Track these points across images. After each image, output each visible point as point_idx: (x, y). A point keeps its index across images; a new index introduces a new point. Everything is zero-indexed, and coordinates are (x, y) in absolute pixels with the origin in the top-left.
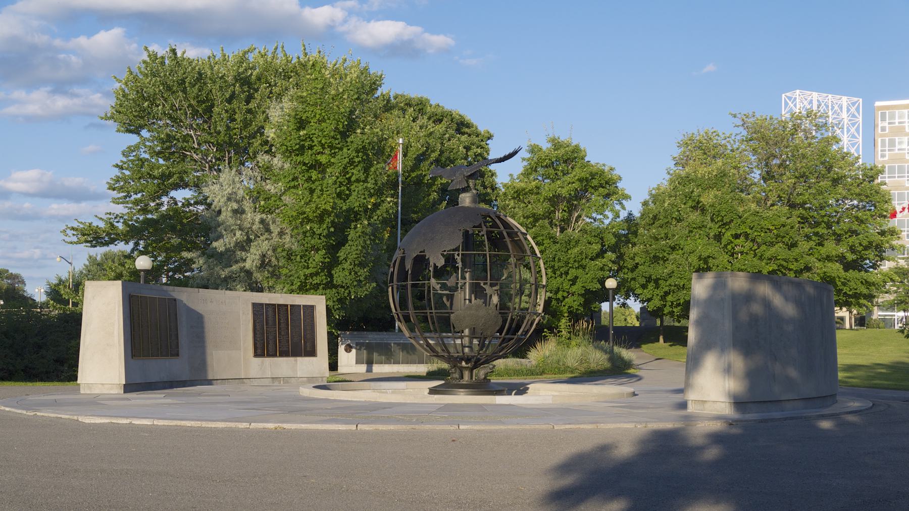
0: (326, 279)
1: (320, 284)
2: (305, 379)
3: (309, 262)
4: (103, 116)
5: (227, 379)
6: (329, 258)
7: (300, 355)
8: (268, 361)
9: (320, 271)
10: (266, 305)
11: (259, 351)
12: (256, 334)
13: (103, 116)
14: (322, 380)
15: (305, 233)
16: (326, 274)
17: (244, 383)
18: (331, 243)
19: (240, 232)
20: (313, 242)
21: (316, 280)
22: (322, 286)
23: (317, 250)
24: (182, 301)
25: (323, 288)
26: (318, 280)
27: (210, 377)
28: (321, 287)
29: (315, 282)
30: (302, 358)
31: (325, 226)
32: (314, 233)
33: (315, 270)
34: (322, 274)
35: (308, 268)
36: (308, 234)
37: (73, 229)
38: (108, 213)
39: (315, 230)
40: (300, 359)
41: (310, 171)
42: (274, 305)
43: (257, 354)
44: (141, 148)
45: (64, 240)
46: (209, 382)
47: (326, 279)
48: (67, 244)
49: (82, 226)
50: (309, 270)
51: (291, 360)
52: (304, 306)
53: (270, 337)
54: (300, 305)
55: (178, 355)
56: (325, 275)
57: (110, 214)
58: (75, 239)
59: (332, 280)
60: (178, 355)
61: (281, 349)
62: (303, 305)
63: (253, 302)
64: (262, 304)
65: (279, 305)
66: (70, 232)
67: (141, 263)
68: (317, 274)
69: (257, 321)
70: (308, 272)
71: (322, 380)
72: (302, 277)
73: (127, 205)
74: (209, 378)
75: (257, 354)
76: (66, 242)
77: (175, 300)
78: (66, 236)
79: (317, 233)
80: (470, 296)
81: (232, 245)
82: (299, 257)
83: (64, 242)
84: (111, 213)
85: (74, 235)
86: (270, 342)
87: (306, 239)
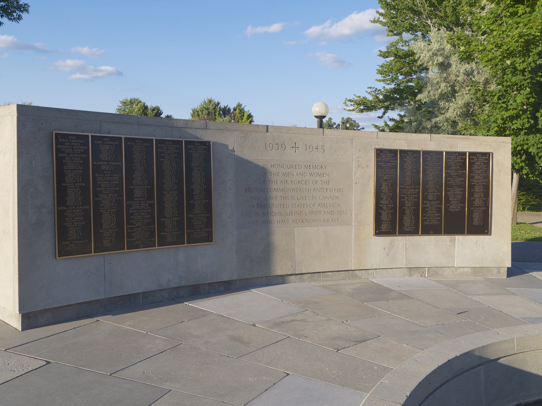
0: (529, 122)
1: (522, 129)
2: (469, 269)
3: (509, 104)
4: (372, 20)
5: (323, 272)
6: (533, 97)
7: (461, 232)
8: (401, 241)
9: (521, 113)
10: (402, 152)
11: (384, 227)
12: (382, 199)
13: (372, 20)
14: (499, 272)
15: (504, 70)
16: (529, 116)
17: (356, 276)
18: (537, 80)
19: (445, 84)
20: (514, 79)
21: (517, 124)
22: (524, 131)
23: (519, 90)
24: (226, 146)
25: (525, 134)
26: (518, 124)
27: (279, 269)
28: (522, 133)
29: (514, 127)
30: (442, 237)
31: (531, 59)
32: (515, 69)
33: (515, 112)
34: (524, 116)
35: (507, 110)
36: (508, 71)
37: (350, 101)
38: (369, 88)
39: (517, 65)
40: (459, 238)
41: (516, 6)
42: (417, 152)
43: (379, 232)
44: (400, 43)
45: (344, 109)
46: (282, 280)
47: (529, 122)
48: (347, 111)
49: (356, 98)
50: (509, 112)
51: (443, 240)
52: (471, 154)
53: (407, 204)
54: (442, 152)
55: (208, 238)
56: (528, 118)
57: (371, 88)
58: (352, 108)
59: (536, 123)
60: (208, 238)
61: (426, 223)
62: (446, 152)
63: (378, 147)
64: (394, 152)
65: (426, 153)
66: (349, 103)
67: (317, 109)
68: (518, 116)
69: (385, 178)
70: (506, 114)
71: (499, 272)
72: (500, 121)
73: (387, 82)
74: (279, 274)
75: (379, 232)
76: (345, 110)
77: (206, 145)
78: (347, 106)
79: (519, 68)
80: (451, 170)
81: (436, 96)
82: (496, 98)
83: (344, 110)
84: (371, 87)
85: (351, 105)
86: (407, 212)
87: (505, 76)
